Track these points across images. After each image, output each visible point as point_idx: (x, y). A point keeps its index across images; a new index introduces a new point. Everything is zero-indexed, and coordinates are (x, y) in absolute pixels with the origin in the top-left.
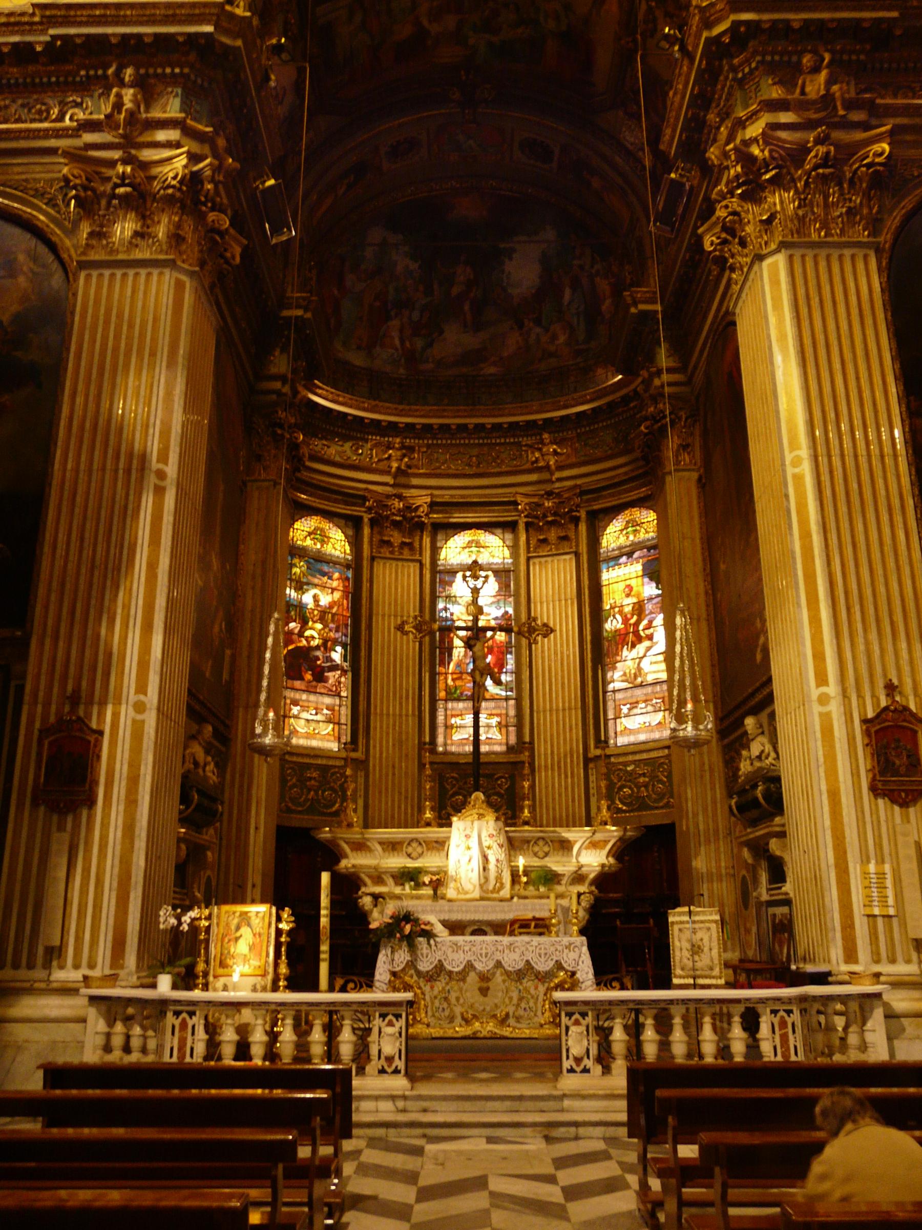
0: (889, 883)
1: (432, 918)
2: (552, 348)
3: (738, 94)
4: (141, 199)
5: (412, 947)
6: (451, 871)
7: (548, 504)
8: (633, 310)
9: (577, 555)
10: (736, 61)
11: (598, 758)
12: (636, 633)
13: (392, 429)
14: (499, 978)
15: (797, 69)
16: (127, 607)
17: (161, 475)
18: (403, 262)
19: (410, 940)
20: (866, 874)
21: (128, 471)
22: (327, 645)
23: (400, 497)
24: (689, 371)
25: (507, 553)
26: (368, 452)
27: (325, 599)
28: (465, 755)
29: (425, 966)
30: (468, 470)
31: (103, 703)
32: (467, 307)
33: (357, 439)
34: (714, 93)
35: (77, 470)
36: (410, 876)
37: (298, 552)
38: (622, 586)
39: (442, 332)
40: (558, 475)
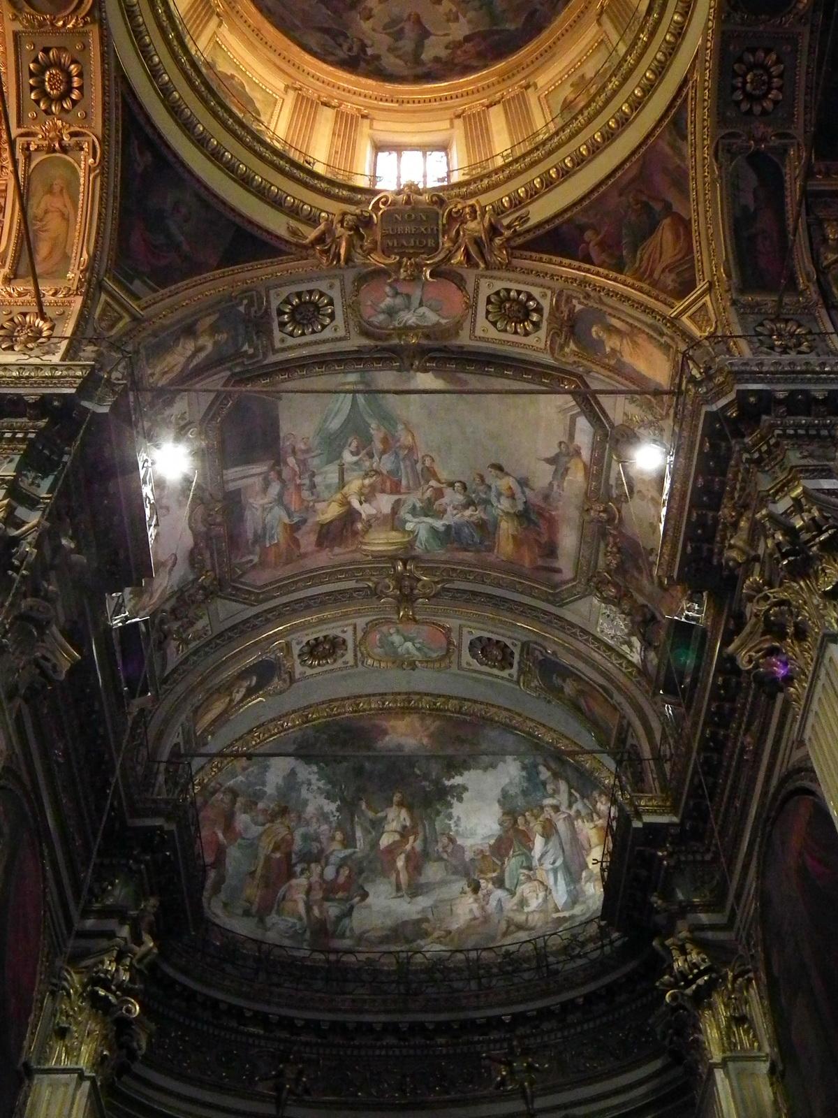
2: (520, 918)
8: (637, 824)
10: (747, 440)
18: (318, 803)
24: (728, 907)
32: (400, 863)
34: (723, 484)
39: (365, 895)
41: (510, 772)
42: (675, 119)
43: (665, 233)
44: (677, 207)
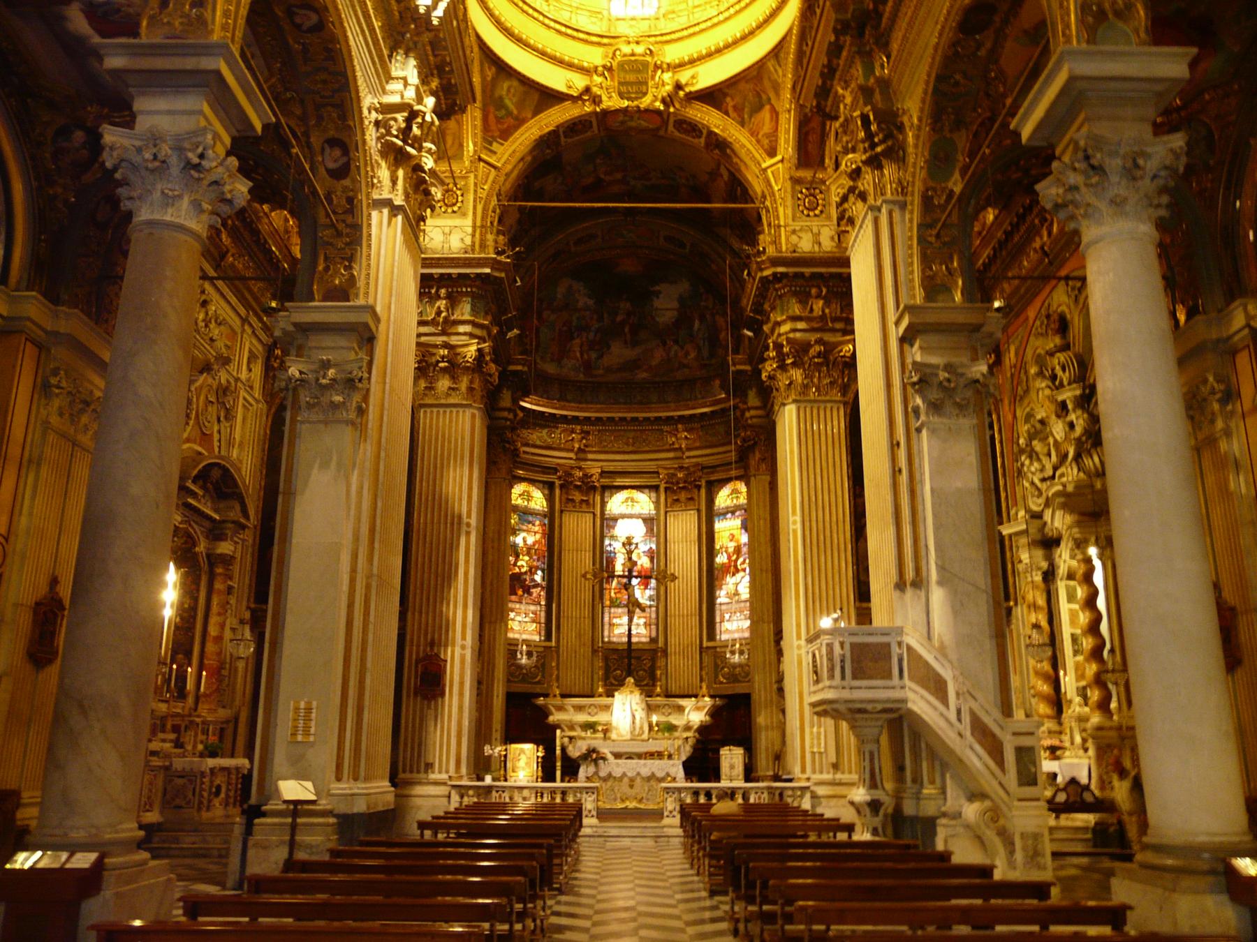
0: (822, 737)
1: (605, 750)
2: (685, 362)
3: (778, 302)
4: (454, 368)
5: (596, 765)
6: (614, 724)
7: (680, 475)
9: (699, 511)
11: (708, 648)
12: (736, 567)
13: (575, 420)
14: (638, 780)
15: (809, 295)
16: (456, 597)
17: (468, 525)
19: (595, 761)
20: (812, 733)
21: (452, 524)
22: (532, 571)
23: (580, 468)
25: (652, 506)
26: (558, 435)
27: (530, 540)
28: (622, 644)
29: (602, 774)
30: (626, 449)
31: (446, 646)
32: (627, 330)
33: (549, 427)
35: (426, 523)
36: (590, 726)
37: (516, 509)
38: (727, 534)
39: (609, 347)
40: (687, 454)
41: (684, 287)
42: (777, 52)
43: (766, 114)
44: (773, 101)
